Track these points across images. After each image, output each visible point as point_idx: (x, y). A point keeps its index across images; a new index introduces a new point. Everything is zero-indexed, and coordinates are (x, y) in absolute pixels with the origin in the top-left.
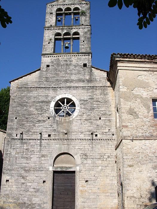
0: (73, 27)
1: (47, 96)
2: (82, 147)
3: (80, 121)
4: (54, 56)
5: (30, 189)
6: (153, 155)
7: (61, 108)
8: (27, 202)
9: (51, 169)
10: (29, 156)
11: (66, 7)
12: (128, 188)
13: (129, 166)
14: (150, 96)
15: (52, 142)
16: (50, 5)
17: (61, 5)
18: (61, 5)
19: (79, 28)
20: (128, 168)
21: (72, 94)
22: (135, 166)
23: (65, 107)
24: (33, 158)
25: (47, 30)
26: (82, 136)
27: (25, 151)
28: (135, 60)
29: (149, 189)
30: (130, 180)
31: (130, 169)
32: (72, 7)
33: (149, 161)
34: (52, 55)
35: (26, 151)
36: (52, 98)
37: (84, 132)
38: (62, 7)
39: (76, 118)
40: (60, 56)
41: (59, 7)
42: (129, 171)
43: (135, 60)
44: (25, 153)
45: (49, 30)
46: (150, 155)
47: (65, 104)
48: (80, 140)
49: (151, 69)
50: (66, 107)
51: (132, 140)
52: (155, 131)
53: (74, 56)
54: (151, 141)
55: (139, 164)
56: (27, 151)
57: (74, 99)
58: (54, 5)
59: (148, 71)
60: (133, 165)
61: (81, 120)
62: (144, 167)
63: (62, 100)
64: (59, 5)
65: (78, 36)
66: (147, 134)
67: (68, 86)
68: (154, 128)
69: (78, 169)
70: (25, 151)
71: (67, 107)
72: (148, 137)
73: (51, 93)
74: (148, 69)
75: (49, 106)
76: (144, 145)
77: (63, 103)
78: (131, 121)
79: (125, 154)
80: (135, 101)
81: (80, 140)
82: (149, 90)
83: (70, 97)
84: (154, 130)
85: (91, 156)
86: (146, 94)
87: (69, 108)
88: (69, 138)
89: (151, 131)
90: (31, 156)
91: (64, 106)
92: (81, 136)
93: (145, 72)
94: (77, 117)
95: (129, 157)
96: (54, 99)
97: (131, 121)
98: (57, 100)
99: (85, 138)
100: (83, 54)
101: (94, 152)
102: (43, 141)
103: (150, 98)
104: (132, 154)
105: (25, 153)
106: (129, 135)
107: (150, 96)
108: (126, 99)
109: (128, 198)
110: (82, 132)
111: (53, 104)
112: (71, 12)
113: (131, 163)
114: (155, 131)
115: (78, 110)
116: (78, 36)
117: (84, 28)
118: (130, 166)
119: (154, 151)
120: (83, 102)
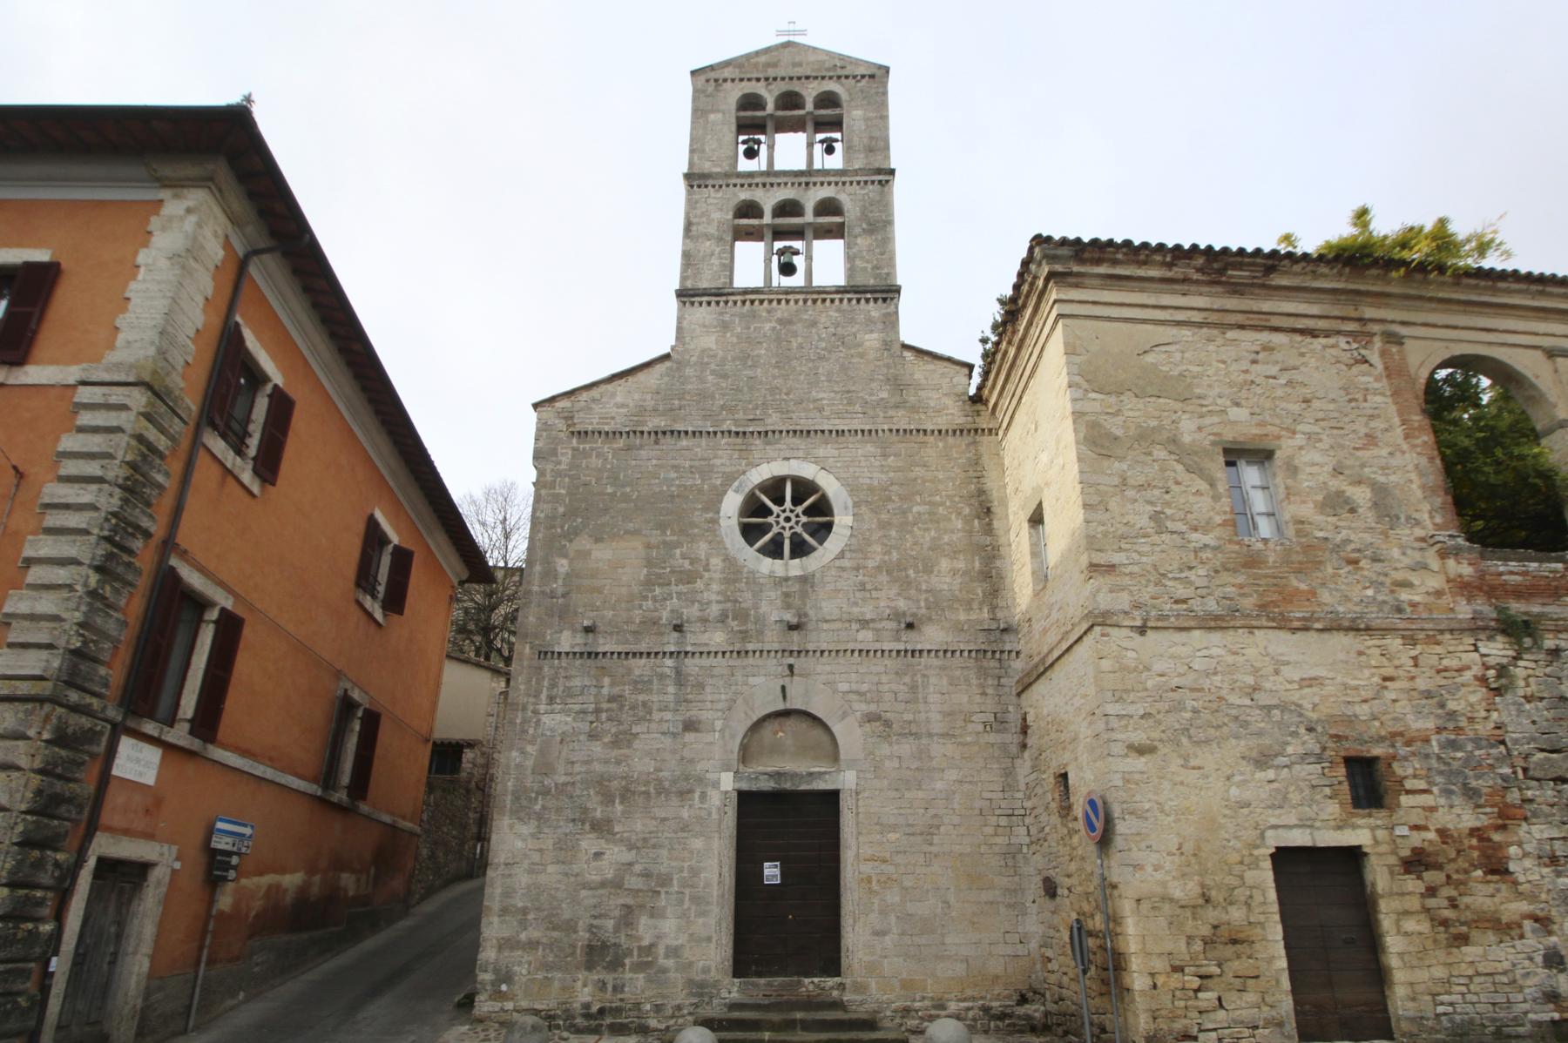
0: (814, 179)
1: (706, 471)
2: (865, 687)
3: (855, 573)
4: (735, 303)
5: (627, 877)
6: (1248, 702)
7: (771, 519)
8: (613, 941)
9: (728, 782)
10: (626, 727)
11: (780, 87)
12: (1137, 855)
13: (1131, 747)
14: (1212, 438)
15: (732, 663)
16: (708, 81)
17: (758, 80)
18: (758, 80)
19: (844, 183)
20: (1129, 760)
21: (816, 463)
22: (1163, 750)
23: (787, 519)
24: (642, 736)
25: (699, 186)
26: (865, 638)
27: (605, 706)
28: (1141, 272)
29: (1241, 863)
30: (1146, 819)
31: (1140, 763)
32: (810, 92)
33: (1233, 726)
34: (724, 298)
35: (609, 705)
36: (729, 479)
37: (873, 620)
38: (760, 89)
39: (838, 563)
40: (762, 302)
41: (749, 88)
42: (1137, 777)
43: (1141, 272)
44: (604, 716)
45: (706, 186)
46: (1234, 699)
47: (788, 504)
48: (856, 654)
49: (1213, 318)
50: (792, 516)
51: (1142, 630)
52: (1246, 590)
53: (824, 300)
54: (1229, 637)
55: (1185, 740)
56: (614, 706)
57: (830, 485)
58: (725, 80)
59: (1200, 325)
60: (1156, 743)
61: (857, 569)
62: (1206, 758)
63: (774, 488)
64: (749, 80)
65: (837, 219)
66: (1212, 605)
67: (798, 428)
68: (1241, 579)
69: (846, 780)
70: (605, 706)
71: (797, 516)
72: (1217, 618)
73: (723, 456)
74: (1197, 317)
75: (718, 512)
76: (1198, 654)
77: (779, 501)
78: (1128, 546)
79: (1110, 694)
80: (1143, 458)
81: (856, 654)
82: (1204, 409)
83: (807, 471)
84: (1241, 586)
85: (910, 722)
86: (1193, 427)
87: (804, 519)
88: (810, 647)
89: (1229, 589)
90: (635, 729)
91: (778, 516)
92: (861, 636)
93: (1186, 333)
94: (841, 555)
95: (1131, 709)
96: (736, 484)
97: (1128, 546)
98: (750, 486)
99: (878, 646)
100: (862, 296)
101: (921, 707)
102: (689, 661)
103: (1213, 444)
104: (1145, 694)
105: (604, 716)
106: (1127, 608)
107: (1212, 438)
108: (1102, 447)
109: (1145, 906)
110: (867, 622)
111: (732, 503)
112: (801, 112)
113: (1139, 737)
114: (1246, 590)
115: (846, 526)
116: (837, 219)
117: (866, 182)
118: (1141, 750)
119: (1250, 680)
120: (866, 498)
